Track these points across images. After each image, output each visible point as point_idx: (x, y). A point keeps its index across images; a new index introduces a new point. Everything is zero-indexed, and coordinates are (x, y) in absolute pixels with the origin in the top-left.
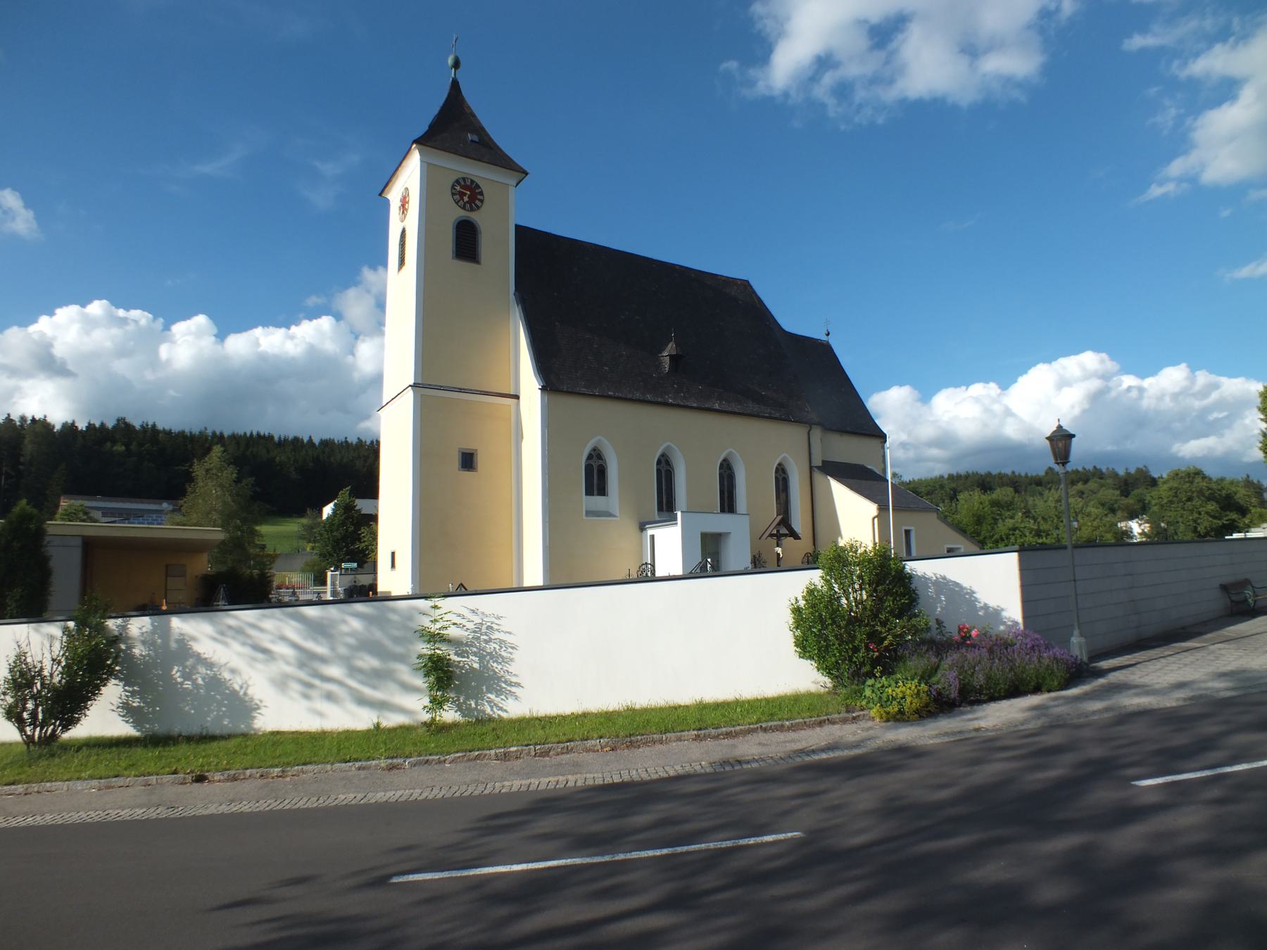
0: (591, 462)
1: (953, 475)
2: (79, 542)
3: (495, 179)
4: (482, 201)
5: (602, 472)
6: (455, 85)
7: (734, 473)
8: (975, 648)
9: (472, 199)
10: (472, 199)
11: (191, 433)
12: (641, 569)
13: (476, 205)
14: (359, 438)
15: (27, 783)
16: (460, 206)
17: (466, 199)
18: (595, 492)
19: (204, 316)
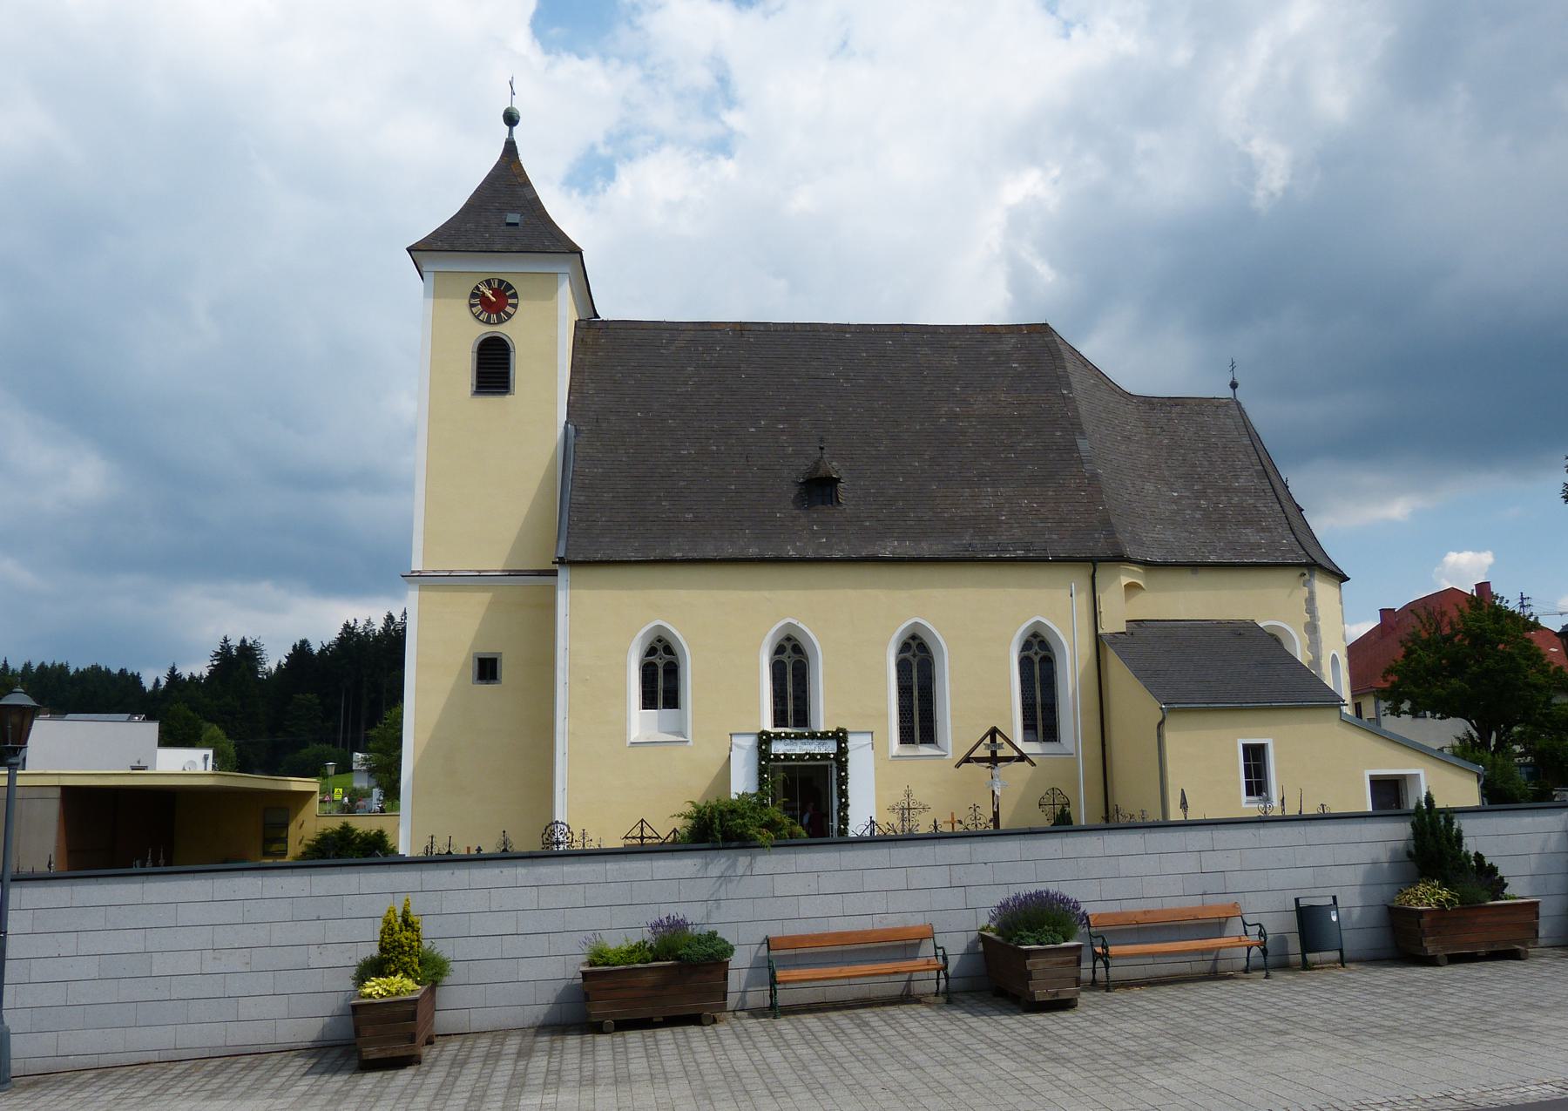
0: (784, 657)
2: (57, 793)
5: (673, 671)
6: (510, 149)
7: (932, 657)
10: (485, 301)
12: (548, 831)
13: (506, 313)
16: (482, 321)
18: (660, 702)
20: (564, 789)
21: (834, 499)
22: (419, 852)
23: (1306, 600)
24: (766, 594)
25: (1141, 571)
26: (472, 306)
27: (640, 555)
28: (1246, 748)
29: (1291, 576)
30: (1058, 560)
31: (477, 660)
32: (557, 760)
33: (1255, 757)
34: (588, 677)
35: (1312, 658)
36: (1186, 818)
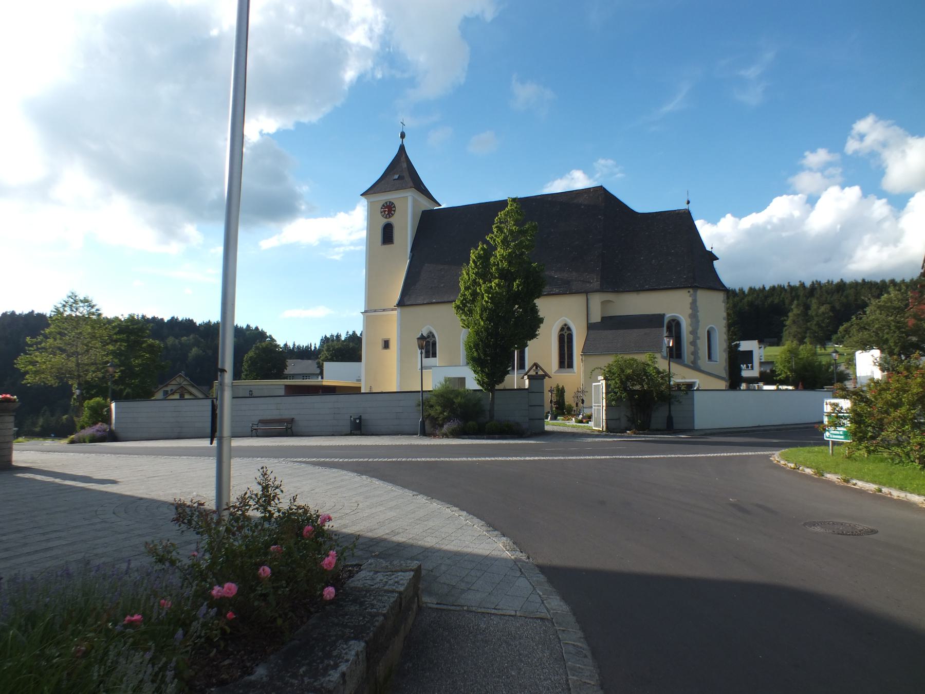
1: (781, 286)
3: (400, 196)
4: (394, 211)
6: (402, 149)
8: (890, 424)
9: (390, 212)
10: (390, 212)
11: (789, 286)
14: (763, 286)
15: (403, 572)
17: (387, 213)
19: (824, 149)
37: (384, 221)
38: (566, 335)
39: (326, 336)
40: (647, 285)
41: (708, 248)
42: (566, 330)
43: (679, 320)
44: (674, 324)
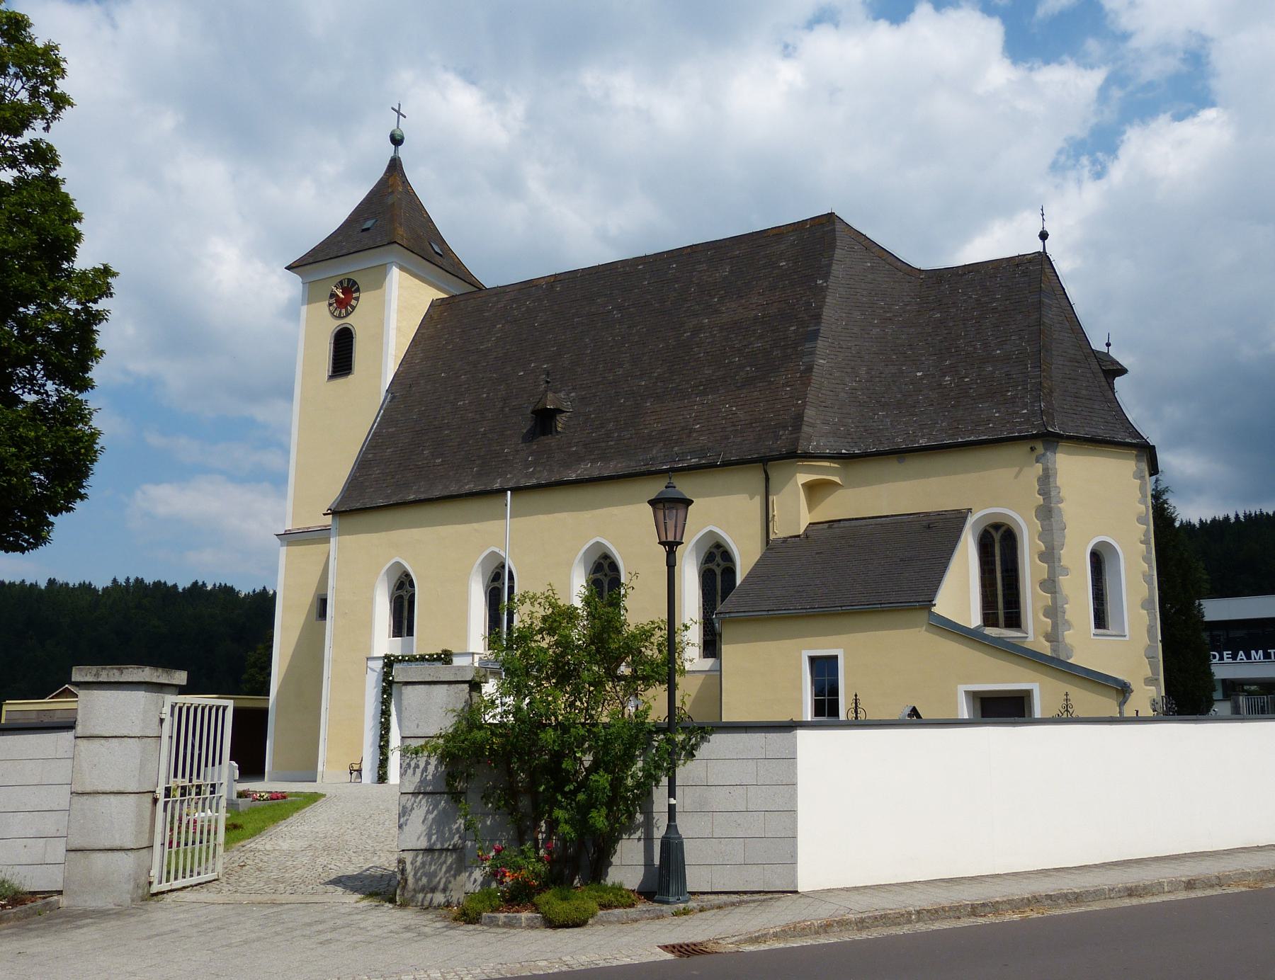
6: (395, 166)
20: (162, 721)
21: (554, 429)
22: (1053, 713)
23: (1039, 479)
24: (475, 525)
25: (836, 465)
26: (330, 305)
27: (385, 501)
28: (813, 660)
29: (1021, 451)
30: (727, 464)
31: (319, 601)
32: (827, 654)
33: (824, 669)
34: (347, 611)
35: (1044, 548)
36: (1137, 715)
37: (334, 325)
38: (718, 571)
39: (84, 582)
40: (922, 437)
41: (1098, 344)
42: (718, 559)
43: (1012, 525)
44: (997, 536)
